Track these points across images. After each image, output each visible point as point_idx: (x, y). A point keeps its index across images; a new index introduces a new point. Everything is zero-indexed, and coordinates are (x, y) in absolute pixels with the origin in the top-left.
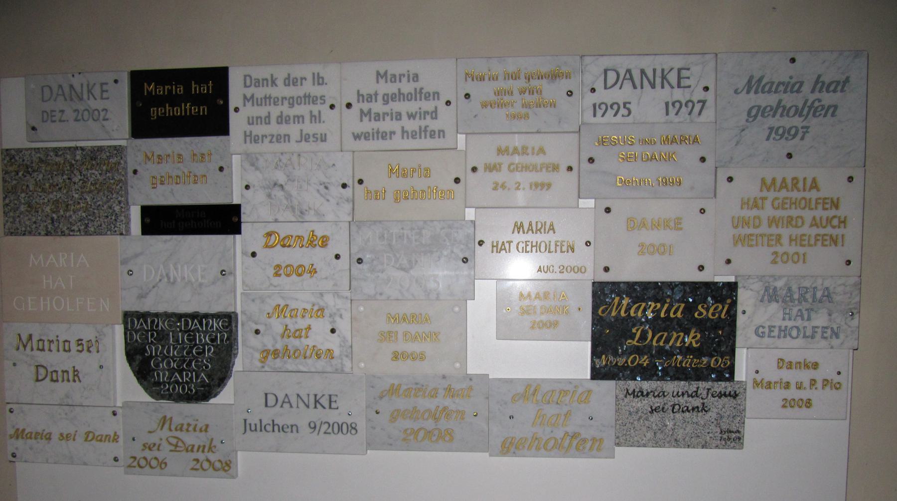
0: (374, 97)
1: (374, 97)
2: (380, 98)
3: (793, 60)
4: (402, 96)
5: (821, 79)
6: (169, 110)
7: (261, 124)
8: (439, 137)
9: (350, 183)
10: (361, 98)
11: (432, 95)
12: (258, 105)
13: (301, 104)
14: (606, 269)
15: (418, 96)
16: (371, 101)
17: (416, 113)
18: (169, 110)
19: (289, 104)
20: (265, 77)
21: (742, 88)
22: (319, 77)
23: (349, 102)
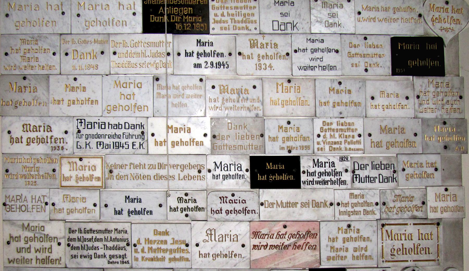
0: (176, 209)
1: (176, 209)
2: (179, 210)
3: (160, 206)
4: (189, 209)
5: (38, 137)
6: (167, 10)
7: (183, 145)
8: (181, 145)
9: (293, 53)
10: (201, 256)
11: (220, 54)
12: (362, 182)
13: (272, 59)
14: (274, 70)
15: (196, 209)
16: (177, 132)
17: (41, 248)
18: (277, 178)
19: (351, 206)
20: (186, 140)
21: (261, 95)
22: (80, 230)
23: (372, 135)
